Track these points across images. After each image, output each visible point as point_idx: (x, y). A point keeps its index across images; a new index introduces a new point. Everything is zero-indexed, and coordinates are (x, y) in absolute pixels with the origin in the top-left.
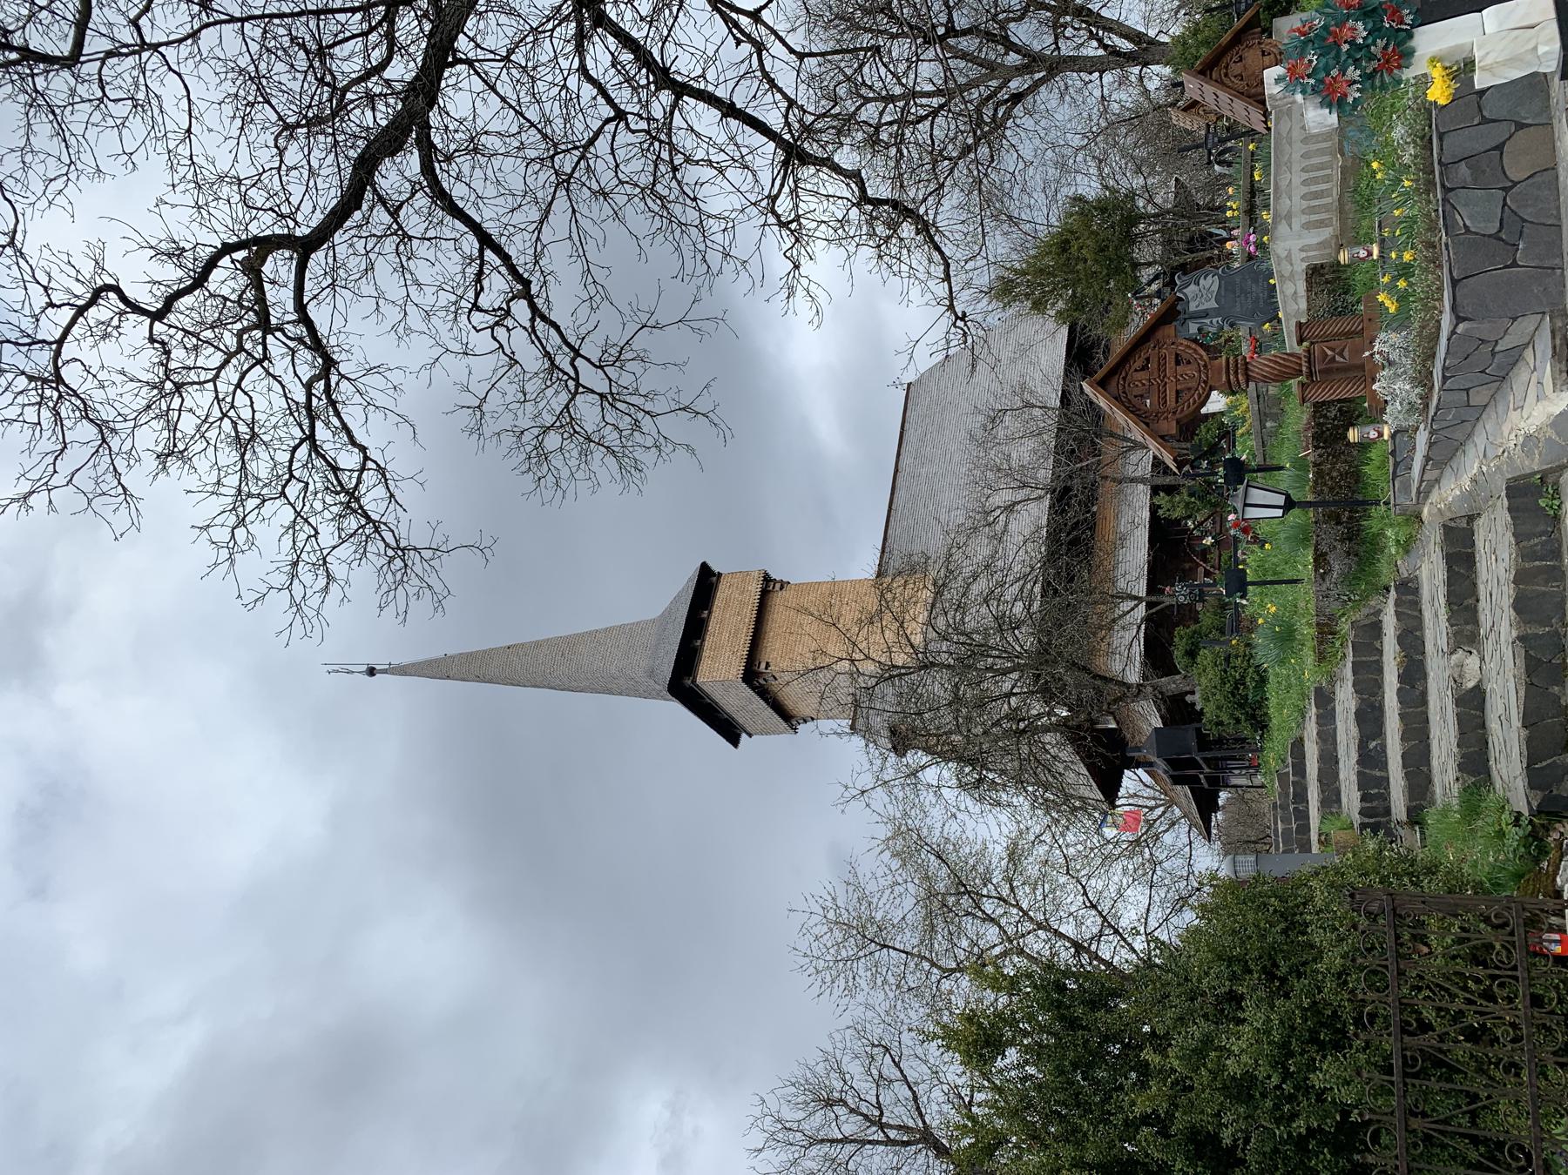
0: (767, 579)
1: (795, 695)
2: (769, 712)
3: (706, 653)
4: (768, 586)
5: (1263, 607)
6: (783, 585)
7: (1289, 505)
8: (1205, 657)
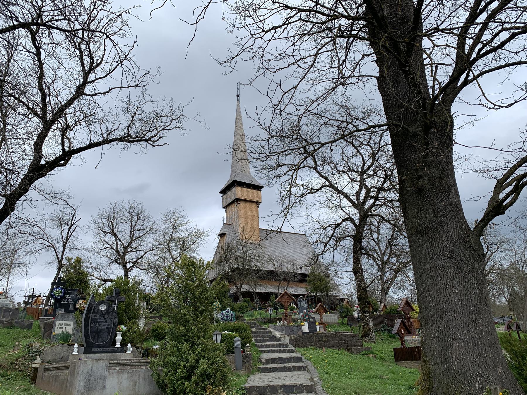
0: (259, 203)
1: (233, 208)
2: (228, 202)
3: (242, 189)
4: (258, 203)
5: (256, 313)
6: (258, 207)
7: (270, 314)
8: (246, 304)
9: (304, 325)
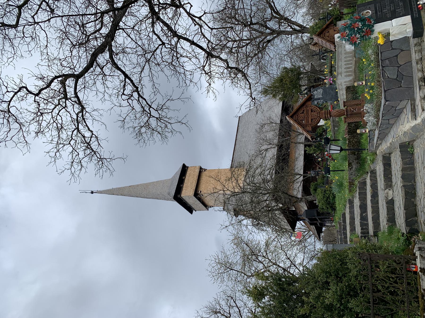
0: (201, 168)
1: (208, 200)
2: (201, 205)
4: (201, 170)
5: (334, 177)
6: (205, 170)
7: (341, 150)
8: (319, 190)
9: (387, 35)
